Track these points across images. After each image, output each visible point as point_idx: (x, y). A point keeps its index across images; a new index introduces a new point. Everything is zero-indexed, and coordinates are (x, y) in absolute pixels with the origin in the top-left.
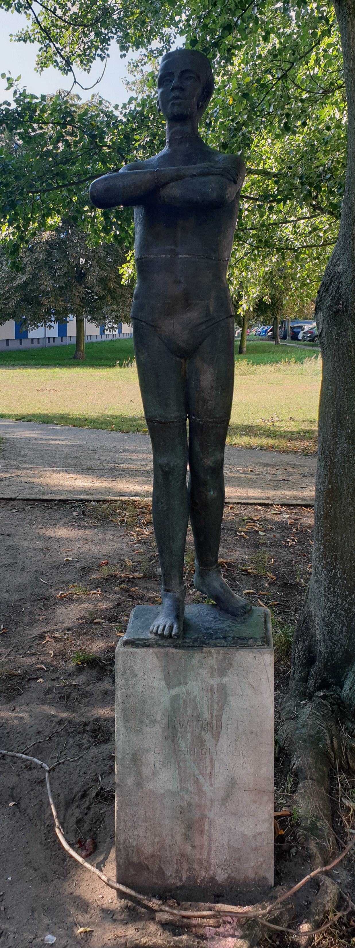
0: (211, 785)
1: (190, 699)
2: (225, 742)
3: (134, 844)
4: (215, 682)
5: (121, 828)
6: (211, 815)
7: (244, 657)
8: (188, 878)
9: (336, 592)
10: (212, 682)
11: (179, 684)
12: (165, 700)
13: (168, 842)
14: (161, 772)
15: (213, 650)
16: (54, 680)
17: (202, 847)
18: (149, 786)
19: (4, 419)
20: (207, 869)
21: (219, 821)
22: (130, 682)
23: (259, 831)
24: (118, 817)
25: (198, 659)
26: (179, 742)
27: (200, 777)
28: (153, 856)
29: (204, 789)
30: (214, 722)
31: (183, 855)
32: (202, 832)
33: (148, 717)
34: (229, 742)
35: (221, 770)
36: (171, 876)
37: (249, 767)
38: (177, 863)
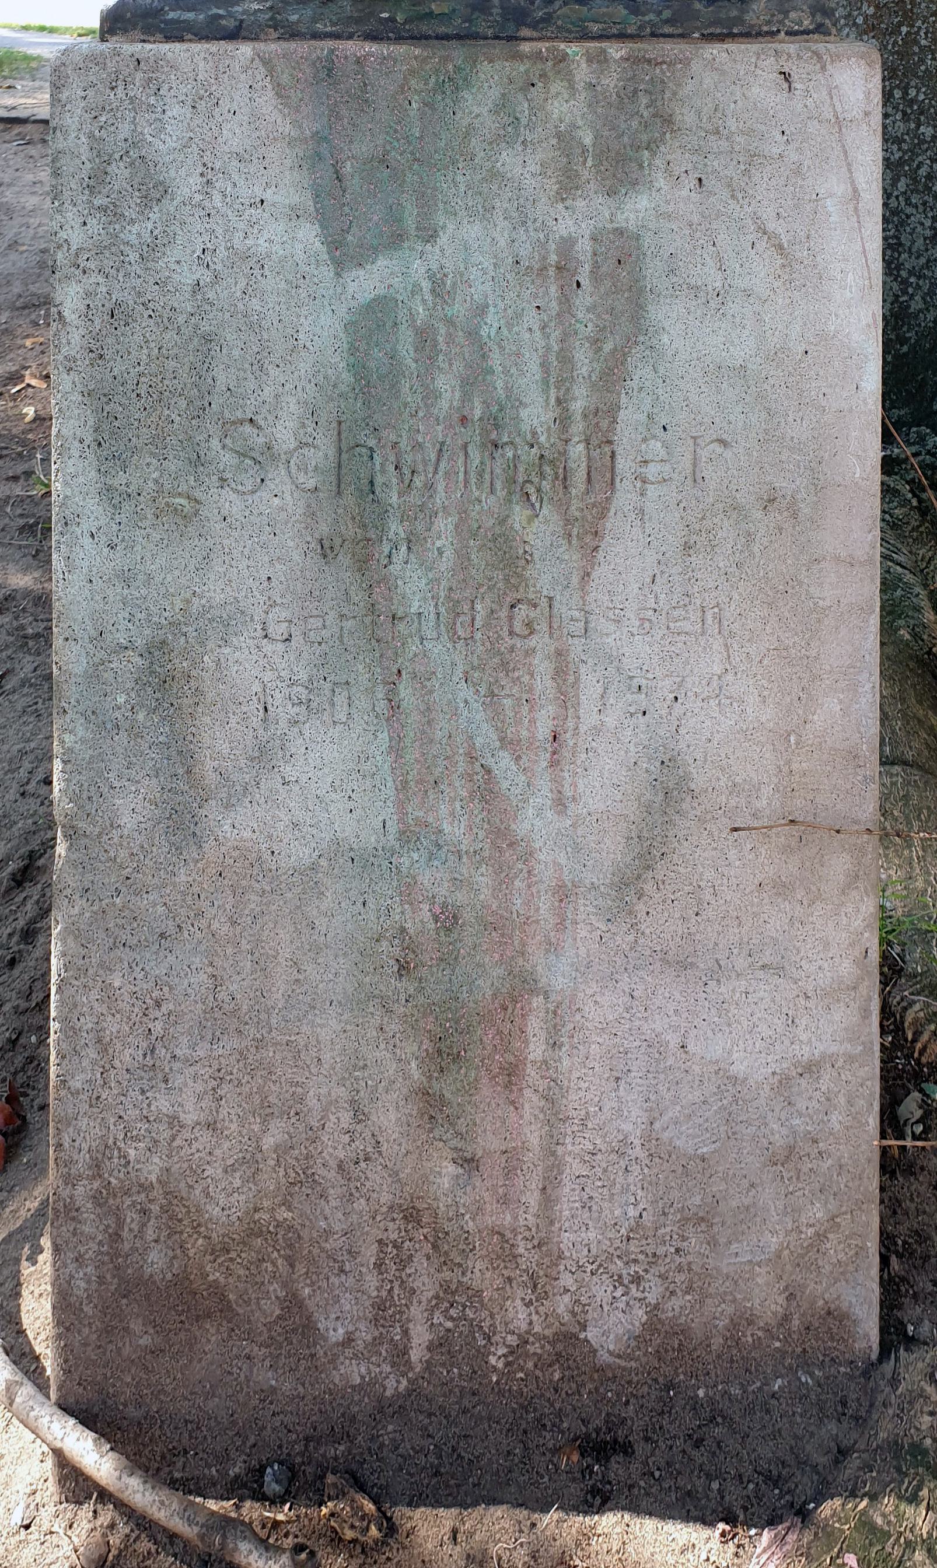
0: (560, 804)
1: (450, 322)
2: (629, 556)
3: (152, 1170)
4: (578, 222)
5: (76, 1084)
6: (557, 974)
7: (732, 81)
8: (440, 1344)
9: (912, 102)
10: (565, 227)
11: (396, 240)
12: (323, 329)
13: (334, 1147)
14: (296, 746)
15: (573, 49)
16: (15, 478)
17: (512, 1162)
18: (234, 827)
19: (55, 35)
20: (538, 1288)
21: (600, 1007)
22: (132, 233)
23: (805, 1053)
24: (64, 1020)
25: (495, 93)
26: (395, 568)
27: (503, 764)
28: (255, 1231)
29: (521, 828)
30: (577, 450)
31: (411, 1215)
32: (511, 1074)
33: (227, 427)
34: (651, 557)
35: (610, 721)
36: (349, 1340)
37: (753, 699)
38: (379, 1265)
